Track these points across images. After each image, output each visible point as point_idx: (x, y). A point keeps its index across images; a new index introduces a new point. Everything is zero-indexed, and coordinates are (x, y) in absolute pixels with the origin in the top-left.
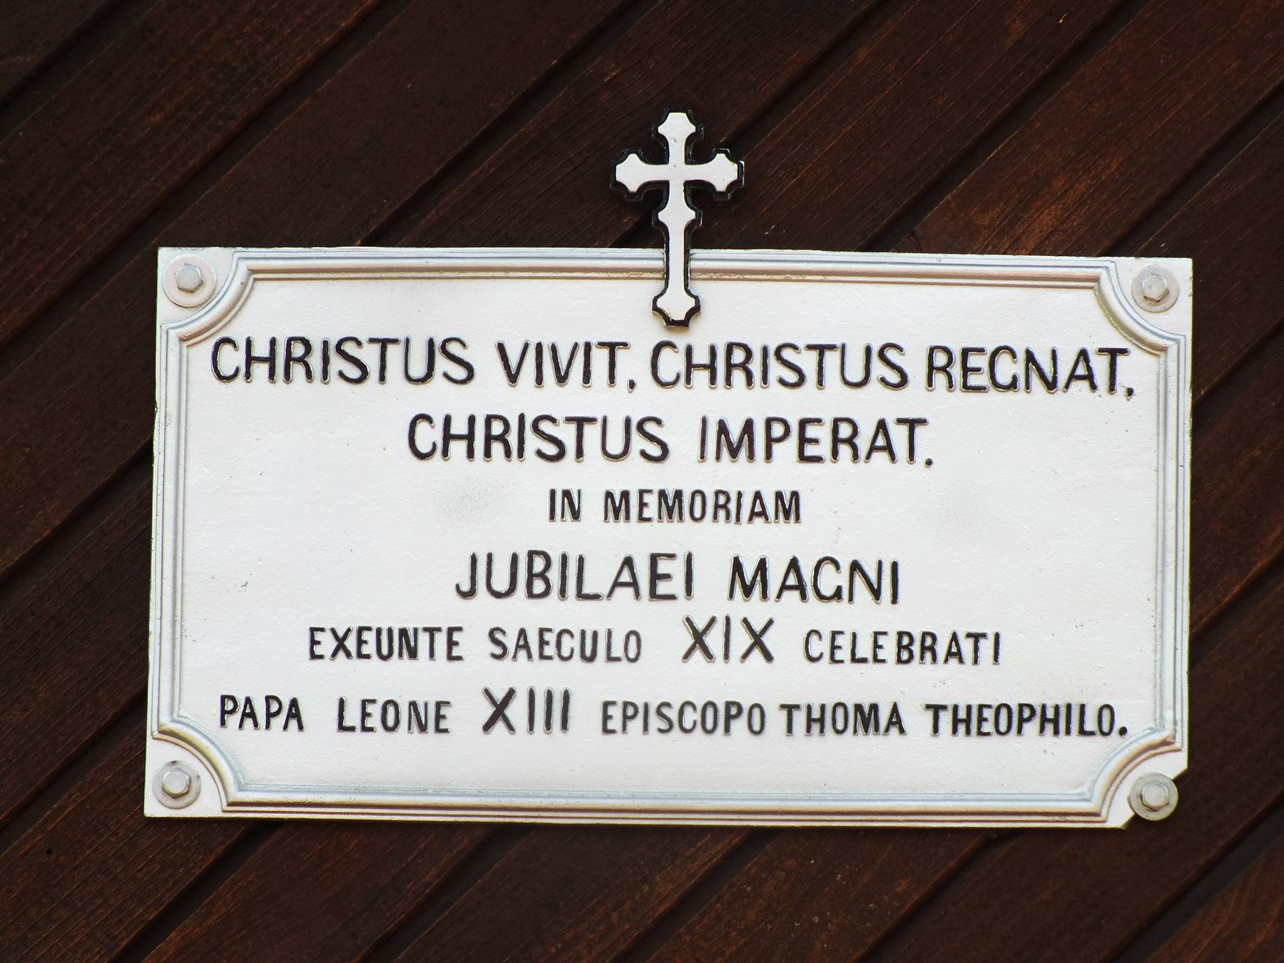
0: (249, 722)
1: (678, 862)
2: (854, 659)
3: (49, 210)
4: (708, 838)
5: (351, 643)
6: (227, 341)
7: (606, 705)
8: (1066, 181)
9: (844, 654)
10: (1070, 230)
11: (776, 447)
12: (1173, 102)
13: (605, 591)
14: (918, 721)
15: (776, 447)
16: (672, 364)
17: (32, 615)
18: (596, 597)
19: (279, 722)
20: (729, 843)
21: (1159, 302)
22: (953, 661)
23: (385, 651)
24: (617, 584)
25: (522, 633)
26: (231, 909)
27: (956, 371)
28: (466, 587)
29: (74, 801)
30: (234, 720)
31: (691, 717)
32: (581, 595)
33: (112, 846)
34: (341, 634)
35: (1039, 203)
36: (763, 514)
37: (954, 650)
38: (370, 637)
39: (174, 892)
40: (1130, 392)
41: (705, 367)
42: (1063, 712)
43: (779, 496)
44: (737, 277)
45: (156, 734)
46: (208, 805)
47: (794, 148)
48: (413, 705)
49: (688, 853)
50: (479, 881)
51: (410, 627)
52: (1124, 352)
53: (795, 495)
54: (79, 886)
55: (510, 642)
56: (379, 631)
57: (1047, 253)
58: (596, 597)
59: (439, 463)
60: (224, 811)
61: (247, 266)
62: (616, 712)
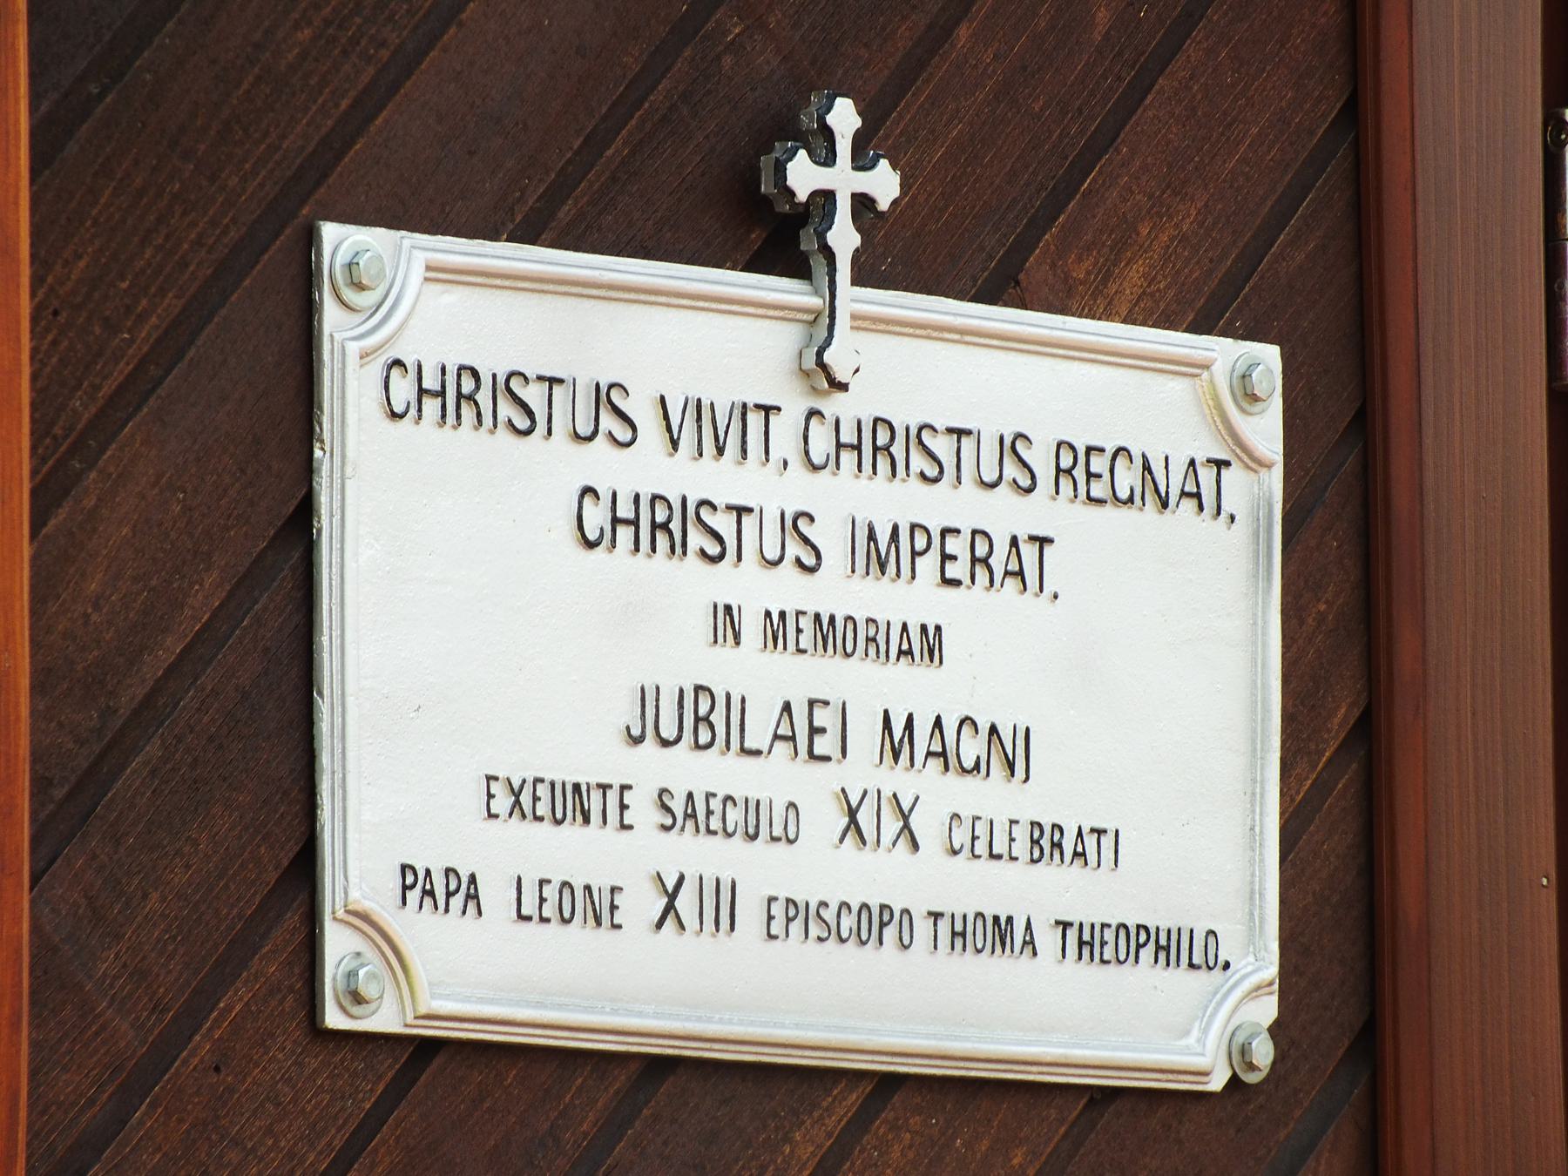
0: (428, 901)
1: (816, 1114)
2: (992, 856)
3: (199, 153)
4: (843, 1085)
5: (526, 799)
6: (398, 363)
7: (771, 900)
8: (1151, 228)
9: (981, 847)
10: (1157, 294)
11: (918, 560)
12: (1242, 135)
13: (765, 749)
14: (643, 811)
15: (918, 560)
16: (821, 444)
17: (191, 732)
18: (758, 753)
19: (457, 902)
20: (863, 1092)
21: (1249, 396)
22: (1079, 862)
23: (559, 815)
24: (776, 737)
25: (690, 796)
26: (395, 1158)
27: (1079, 473)
28: (636, 732)
29: (241, 999)
30: (414, 896)
31: (848, 922)
32: (745, 751)
33: (280, 1065)
34: (516, 784)
35: (1129, 254)
36: (910, 652)
37: (1080, 849)
38: (543, 791)
39: (345, 1134)
40: (1232, 518)
41: (852, 447)
42: (1174, 937)
43: (924, 628)
44: (781, 314)
45: (340, 913)
46: (384, 1019)
47: (905, 155)
48: (588, 888)
49: (825, 1104)
50: (629, 1132)
51: (582, 780)
52: (1227, 464)
53: (938, 628)
54: (249, 1118)
55: (678, 806)
56: (553, 785)
57: (1138, 323)
58: (758, 753)
59: (604, 555)
60: (406, 1026)
61: (427, 260)
62: (778, 909)
